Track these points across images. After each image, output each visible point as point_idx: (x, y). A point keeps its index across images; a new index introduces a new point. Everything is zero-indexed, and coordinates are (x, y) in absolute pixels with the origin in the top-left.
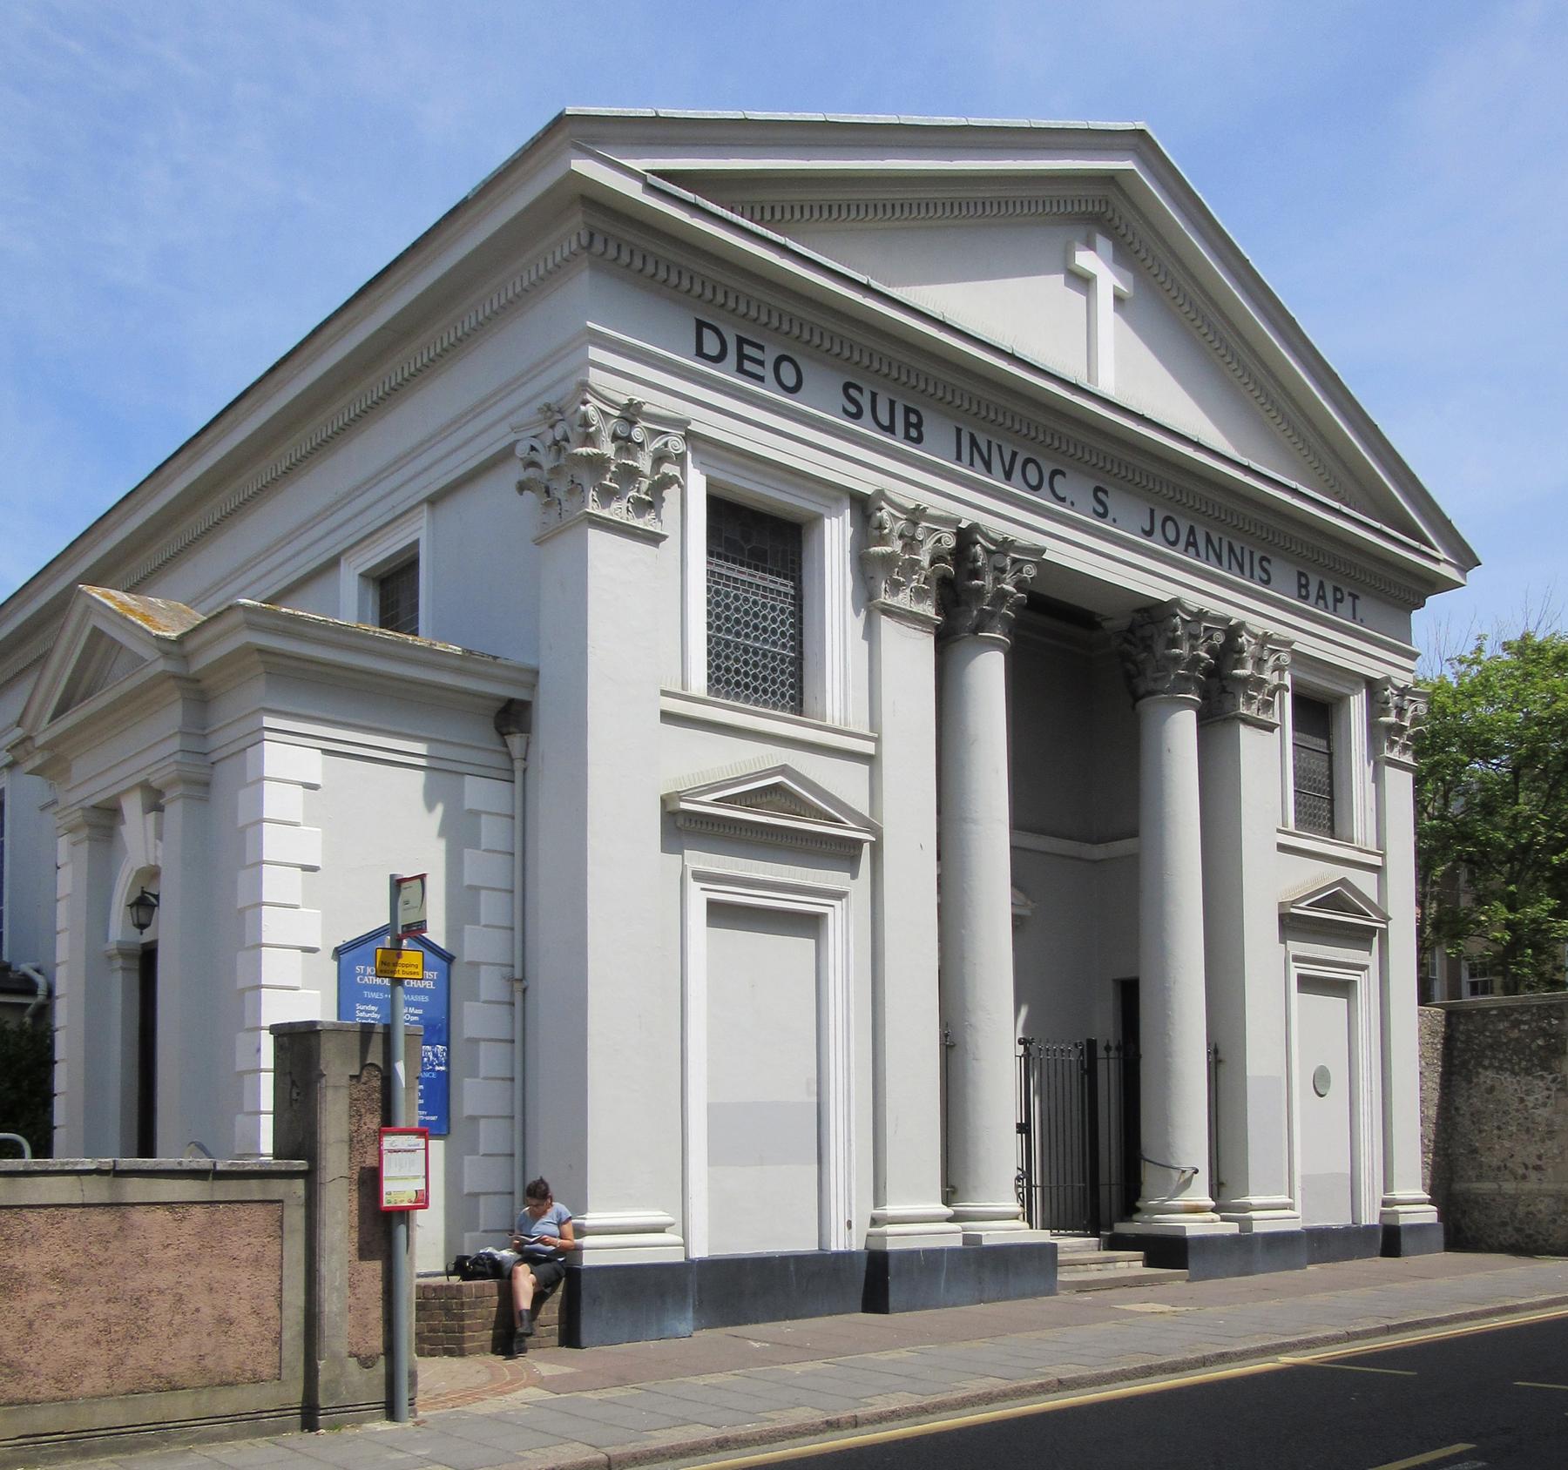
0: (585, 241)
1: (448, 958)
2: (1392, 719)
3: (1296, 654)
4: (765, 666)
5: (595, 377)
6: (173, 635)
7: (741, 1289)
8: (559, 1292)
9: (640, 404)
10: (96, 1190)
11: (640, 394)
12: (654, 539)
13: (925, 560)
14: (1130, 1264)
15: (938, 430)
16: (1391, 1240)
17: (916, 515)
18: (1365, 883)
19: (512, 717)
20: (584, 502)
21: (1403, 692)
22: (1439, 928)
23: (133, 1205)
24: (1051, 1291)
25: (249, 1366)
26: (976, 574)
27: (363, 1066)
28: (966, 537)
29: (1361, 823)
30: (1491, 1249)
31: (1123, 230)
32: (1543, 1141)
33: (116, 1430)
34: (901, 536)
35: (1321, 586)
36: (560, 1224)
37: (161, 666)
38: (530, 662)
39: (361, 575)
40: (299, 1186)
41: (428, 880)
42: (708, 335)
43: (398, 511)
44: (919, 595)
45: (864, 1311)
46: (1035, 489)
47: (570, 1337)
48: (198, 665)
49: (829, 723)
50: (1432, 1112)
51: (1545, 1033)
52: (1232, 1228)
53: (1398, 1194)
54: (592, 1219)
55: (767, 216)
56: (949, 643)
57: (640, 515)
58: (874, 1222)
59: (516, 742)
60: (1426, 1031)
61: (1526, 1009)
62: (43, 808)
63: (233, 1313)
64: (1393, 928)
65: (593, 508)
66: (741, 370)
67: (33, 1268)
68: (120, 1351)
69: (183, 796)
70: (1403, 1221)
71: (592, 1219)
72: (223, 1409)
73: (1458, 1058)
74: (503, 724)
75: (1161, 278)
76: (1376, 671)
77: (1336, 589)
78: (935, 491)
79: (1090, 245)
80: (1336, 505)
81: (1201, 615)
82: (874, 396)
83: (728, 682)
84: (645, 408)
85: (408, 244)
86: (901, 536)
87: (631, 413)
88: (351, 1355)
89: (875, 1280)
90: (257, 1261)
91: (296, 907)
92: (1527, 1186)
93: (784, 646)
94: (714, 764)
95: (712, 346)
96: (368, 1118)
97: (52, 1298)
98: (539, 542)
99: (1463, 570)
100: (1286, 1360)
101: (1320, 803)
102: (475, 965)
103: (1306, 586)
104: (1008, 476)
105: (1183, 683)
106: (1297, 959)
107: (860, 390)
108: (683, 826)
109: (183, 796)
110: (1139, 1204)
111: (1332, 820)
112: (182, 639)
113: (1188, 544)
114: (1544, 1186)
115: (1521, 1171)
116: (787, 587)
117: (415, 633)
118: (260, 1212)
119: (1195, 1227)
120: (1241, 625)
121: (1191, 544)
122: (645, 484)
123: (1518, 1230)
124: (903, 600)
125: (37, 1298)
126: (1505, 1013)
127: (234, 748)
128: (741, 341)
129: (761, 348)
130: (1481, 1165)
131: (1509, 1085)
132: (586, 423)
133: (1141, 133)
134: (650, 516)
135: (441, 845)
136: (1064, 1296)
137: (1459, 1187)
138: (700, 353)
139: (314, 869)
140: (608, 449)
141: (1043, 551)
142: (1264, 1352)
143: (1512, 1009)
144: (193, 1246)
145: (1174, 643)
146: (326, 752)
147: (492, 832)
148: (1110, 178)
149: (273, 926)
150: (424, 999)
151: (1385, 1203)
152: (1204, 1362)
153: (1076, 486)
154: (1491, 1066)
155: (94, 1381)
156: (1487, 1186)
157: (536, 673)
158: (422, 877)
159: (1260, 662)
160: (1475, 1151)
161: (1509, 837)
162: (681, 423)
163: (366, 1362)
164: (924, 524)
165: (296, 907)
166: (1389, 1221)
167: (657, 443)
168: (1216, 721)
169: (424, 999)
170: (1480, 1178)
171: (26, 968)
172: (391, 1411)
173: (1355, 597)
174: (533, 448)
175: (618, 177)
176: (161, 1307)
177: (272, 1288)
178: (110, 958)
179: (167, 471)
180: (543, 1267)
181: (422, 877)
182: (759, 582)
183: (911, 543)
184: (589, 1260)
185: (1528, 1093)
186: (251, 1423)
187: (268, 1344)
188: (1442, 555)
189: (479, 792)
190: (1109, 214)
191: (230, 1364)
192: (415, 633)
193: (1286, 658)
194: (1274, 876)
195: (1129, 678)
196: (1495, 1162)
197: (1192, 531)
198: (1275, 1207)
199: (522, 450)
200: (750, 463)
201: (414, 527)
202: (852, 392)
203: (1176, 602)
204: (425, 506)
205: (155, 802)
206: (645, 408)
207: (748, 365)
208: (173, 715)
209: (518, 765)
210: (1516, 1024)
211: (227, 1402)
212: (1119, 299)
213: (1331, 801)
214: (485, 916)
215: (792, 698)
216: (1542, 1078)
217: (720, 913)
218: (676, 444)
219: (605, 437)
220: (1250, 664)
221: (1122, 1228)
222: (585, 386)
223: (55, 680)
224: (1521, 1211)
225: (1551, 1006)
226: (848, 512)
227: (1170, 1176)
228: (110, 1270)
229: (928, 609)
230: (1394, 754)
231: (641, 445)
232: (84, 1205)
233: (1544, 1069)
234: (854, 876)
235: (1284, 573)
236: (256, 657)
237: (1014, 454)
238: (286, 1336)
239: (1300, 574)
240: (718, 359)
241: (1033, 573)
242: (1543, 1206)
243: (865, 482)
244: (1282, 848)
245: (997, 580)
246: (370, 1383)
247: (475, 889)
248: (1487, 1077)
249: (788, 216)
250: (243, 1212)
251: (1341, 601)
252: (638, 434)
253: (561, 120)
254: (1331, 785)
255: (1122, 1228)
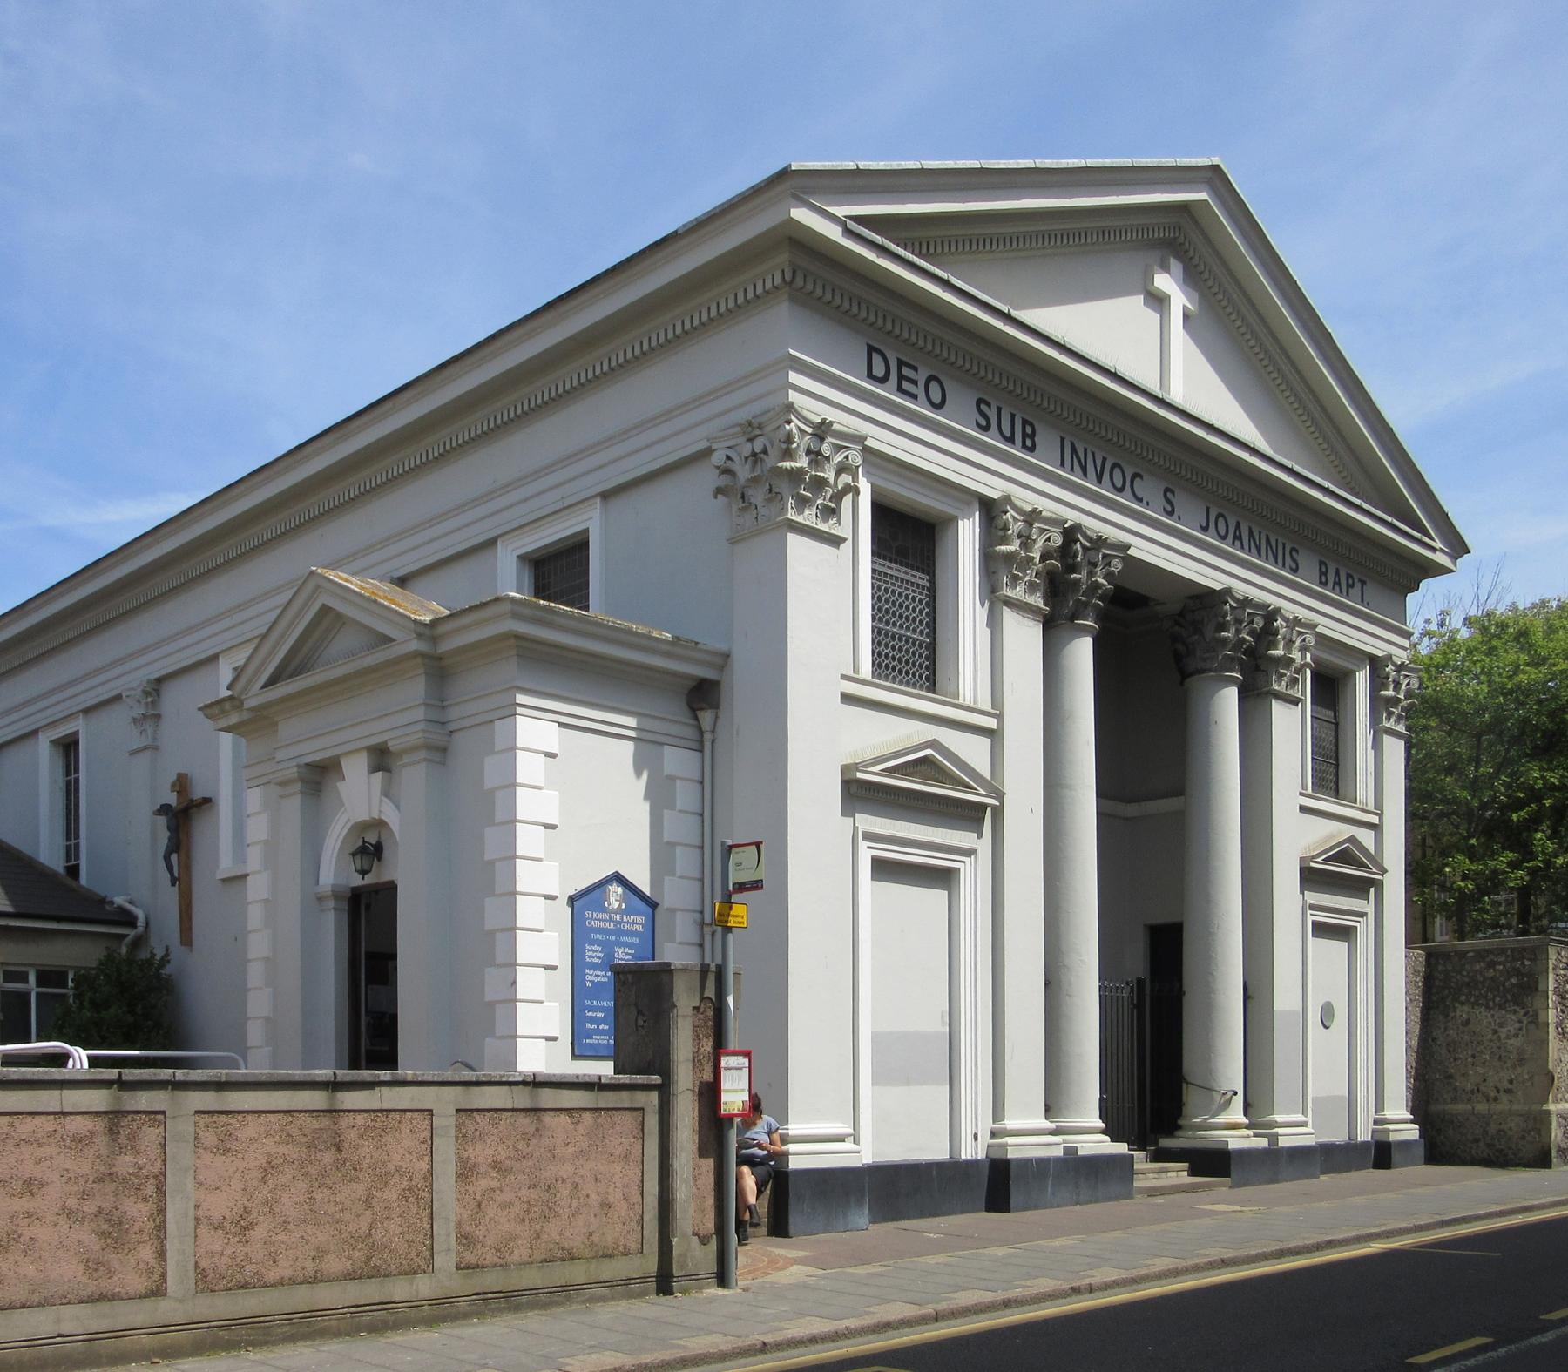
0: (788, 277)
1: (652, 904)
2: (1391, 693)
3: (1320, 636)
4: (907, 651)
5: (793, 396)
6: (427, 619)
7: (900, 1190)
8: (768, 1192)
9: (831, 423)
10: (316, 1099)
11: (831, 414)
12: (836, 541)
13: (1037, 555)
14: (1177, 1174)
15: (1047, 439)
16: (1382, 1154)
17: (1032, 517)
18: (1366, 838)
19: (702, 695)
20: (784, 510)
21: (1400, 668)
22: (1417, 875)
23: (545, 1110)
24: (1129, 1196)
25: (622, 1242)
26: (1074, 568)
27: (703, 999)
28: (1071, 534)
29: (1364, 788)
30: (1463, 1162)
31: (1191, 253)
32: (1514, 1067)
33: (535, 1291)
34: (1019, 536)
35: (1337, 573)
36: (770, 1133)
37: (415, 645)
38: (722, 646)
39: (521, 557)
40: (654, 1096)
41: (763, 847)
42: (876, 358)
43: (568, 502)
44: (1032, 588)
45: (988, 1209)
46: (1120, 490)
47: (779, 1227)
48: (445, 647)
49: (961, 701)
50: (1415, 1043)
51: (1518, 973)
52: (1263, 1143)
53: (1389, 1113)
54: (794, 1129)
55: (924, 251)
56: (1054, 627)
57: (825, 520)
58: (993, 1134)
59: (706, 717)
60: (1411, 971)
61: (1503, 951)
62: (133, 753)
63: (611, 1199)
64: (1387, 879)
65: (791, 515)
66: (900, 390)
67: (480, 1160)
68: (537, 1227)
69: (425, 760)
70: (1393, 1137)
71: (794, 1129)
72: (604, 1277)
73: (1437, 992)
74: (698, 702)
75: (1220, 296)
76: (1378, 649)
77: (1349, 576)
78: (1046, 495)
79: (1165, 268)
80: (1358, 502)
81: (1246, 602)
82: (999, 410)
83: (887, 667)
84: (835, 426)
85: (608, 266)
86: (1019, 536)
87: (822, 430)
88: (694, 1234)
89: (997, 1184)
90: (626, 1157)
91: (540, 860)
92: (1499, 1107)
93: (922, 633)
94: (880, 738)
95: (879, 371)
96: (704, 1041)
97: (494, 1184)
98: (733, 541)
99: (1454, 558)
100: (1377, 1247)
101: (1331, 770)
102: (672, 911)
103: (1325, 574)
104: (1099, 480)
105: (1229, 663)
106: (1313, 907)
107: (989, 405)
108: (859, 793)
109: (425, 760)
110: (1180, 1122)
111: (1337, 783)
112: (435, 623)
113: (1235, 538)
114: (1515, 1107)
115: (1493, 1094)
116: (922, 579)
117: (586, 608)
118: (628, 1116)
119: (1238, 1140)
120: (1278, 610)
121: (1238, 538)
122: (830, 492)
123: (1489, 1145)
124: (1019, 592)
125: (483, 1183)
126: (1481, 954)
127: (466, 723)
128: (901, 363)
129: (915, 369)
130: (1455, 1089)
131: (1484, 1019)
132: (789, 439)
133: (1216, 168)
134: (832, 521)
135: (647, 806)
136: (1138, 1199)
137: (1433, 1108)
138: (870, 376)
139: (553, 827)
140: (802, 462)
141: (1128, 547)
142: (1359, 1240)
143: (1488, 952)
144: (585, 1145)
145: (1223, 627)
146: (561, 725)
147: (685, 796)
148: (1184, 207)
149: (527, 877)
150: (634, 940)
151: (1376, 1122)
152: (1318, 1247)
153: (1150, 487)
154: (1468, 1000)
155: (521, 1252)
156: (1461, 1107)
157: (727, 656)
158: (758, 845)
159: (1289, 643)
160: (1451, 1077)
161: (1473, 797)
162: (859, 439)
163: (704, 1241)
164: (830, 439)
165: (540, 860)
166: (1381, 1138)
167: (839, 458)
168: (1255, 698)
169: (634, 940)
170: (1454, 1100)
171: (119, 900)
172: (722, 1279)
173: (1363, 583)
174: (728, 457)
175: (820, 222)
176: (564, 1191)
177: (637, 1179)
178: (320, 899)
179: (309, 449)
180: (760, 1169)
181: (758, 845)
182: (902, 575)
183: (1026, 542)
184: (794, 1164)
185: (1501, 1025)
186: (622, 1287)
187: (634, 1224)
188: (1438, 545)
189: (678, 761)
190: (1181, 240)
191: (609, 1239)
192: (586, 608)
193: (1311, 639)
194: (1298, 835)
195: (1178, 658)
196: (1469, 1087)
197: (1238, 526)
198: (1297, 1128)
199: (718, 458)
200: (909, 474)
201: (585, 517)
202: (983, 407)
203: (1228, 591)
204: (598, 500)
205: (381, 759)
206: (835, 426)
207: (906, 385)
208: (415, 688)
209: (708, 737)
210: (1492, 965)
211: (609, 1270)
212: (1186, 317)
213: (1337, 766)
214: (680, 869)
215: (927, 679)
216: (1515, 1012)
217: (883, 869)
218: (856, 457)
219: (802, 452)
220: (1281, 646)
221: (1166, 1143)
222: (790, 407)
223: (271, 653)
224: (1493, 1128)
225: (1524, 949)
226: (977, 514)
227: (1212, 1098)
228: (530, 1163)
229: (1037, 600)
230: (1391, 724)
231: (827, 458)
232: (513, 1110)
233: (1516, 1003)
234: (980, 836)
235: (1309, 562)
236: (512, 641)
237: (1104, 460)
238: (646, 1218)
239: (1322, 563)
240: (882, 380)
241: (1120, 567)
242: (1513, 1125)
243: (993, 488)
244: (1303, 809)
245: (1091, 574)
246: (705, 1257)
247: (672, 845)
248: (1463, 1012)
249: (939, 249)
250: (617, 1117)
251: (1352, 586)
252: (826, 449)
253: (785, 174)
254: (1337, 752)
255: (1166, 1143)
